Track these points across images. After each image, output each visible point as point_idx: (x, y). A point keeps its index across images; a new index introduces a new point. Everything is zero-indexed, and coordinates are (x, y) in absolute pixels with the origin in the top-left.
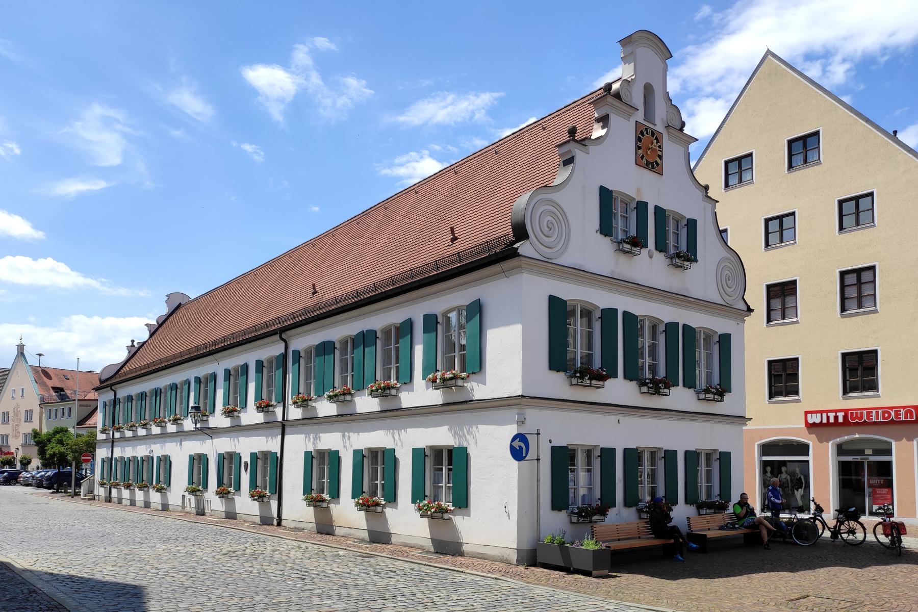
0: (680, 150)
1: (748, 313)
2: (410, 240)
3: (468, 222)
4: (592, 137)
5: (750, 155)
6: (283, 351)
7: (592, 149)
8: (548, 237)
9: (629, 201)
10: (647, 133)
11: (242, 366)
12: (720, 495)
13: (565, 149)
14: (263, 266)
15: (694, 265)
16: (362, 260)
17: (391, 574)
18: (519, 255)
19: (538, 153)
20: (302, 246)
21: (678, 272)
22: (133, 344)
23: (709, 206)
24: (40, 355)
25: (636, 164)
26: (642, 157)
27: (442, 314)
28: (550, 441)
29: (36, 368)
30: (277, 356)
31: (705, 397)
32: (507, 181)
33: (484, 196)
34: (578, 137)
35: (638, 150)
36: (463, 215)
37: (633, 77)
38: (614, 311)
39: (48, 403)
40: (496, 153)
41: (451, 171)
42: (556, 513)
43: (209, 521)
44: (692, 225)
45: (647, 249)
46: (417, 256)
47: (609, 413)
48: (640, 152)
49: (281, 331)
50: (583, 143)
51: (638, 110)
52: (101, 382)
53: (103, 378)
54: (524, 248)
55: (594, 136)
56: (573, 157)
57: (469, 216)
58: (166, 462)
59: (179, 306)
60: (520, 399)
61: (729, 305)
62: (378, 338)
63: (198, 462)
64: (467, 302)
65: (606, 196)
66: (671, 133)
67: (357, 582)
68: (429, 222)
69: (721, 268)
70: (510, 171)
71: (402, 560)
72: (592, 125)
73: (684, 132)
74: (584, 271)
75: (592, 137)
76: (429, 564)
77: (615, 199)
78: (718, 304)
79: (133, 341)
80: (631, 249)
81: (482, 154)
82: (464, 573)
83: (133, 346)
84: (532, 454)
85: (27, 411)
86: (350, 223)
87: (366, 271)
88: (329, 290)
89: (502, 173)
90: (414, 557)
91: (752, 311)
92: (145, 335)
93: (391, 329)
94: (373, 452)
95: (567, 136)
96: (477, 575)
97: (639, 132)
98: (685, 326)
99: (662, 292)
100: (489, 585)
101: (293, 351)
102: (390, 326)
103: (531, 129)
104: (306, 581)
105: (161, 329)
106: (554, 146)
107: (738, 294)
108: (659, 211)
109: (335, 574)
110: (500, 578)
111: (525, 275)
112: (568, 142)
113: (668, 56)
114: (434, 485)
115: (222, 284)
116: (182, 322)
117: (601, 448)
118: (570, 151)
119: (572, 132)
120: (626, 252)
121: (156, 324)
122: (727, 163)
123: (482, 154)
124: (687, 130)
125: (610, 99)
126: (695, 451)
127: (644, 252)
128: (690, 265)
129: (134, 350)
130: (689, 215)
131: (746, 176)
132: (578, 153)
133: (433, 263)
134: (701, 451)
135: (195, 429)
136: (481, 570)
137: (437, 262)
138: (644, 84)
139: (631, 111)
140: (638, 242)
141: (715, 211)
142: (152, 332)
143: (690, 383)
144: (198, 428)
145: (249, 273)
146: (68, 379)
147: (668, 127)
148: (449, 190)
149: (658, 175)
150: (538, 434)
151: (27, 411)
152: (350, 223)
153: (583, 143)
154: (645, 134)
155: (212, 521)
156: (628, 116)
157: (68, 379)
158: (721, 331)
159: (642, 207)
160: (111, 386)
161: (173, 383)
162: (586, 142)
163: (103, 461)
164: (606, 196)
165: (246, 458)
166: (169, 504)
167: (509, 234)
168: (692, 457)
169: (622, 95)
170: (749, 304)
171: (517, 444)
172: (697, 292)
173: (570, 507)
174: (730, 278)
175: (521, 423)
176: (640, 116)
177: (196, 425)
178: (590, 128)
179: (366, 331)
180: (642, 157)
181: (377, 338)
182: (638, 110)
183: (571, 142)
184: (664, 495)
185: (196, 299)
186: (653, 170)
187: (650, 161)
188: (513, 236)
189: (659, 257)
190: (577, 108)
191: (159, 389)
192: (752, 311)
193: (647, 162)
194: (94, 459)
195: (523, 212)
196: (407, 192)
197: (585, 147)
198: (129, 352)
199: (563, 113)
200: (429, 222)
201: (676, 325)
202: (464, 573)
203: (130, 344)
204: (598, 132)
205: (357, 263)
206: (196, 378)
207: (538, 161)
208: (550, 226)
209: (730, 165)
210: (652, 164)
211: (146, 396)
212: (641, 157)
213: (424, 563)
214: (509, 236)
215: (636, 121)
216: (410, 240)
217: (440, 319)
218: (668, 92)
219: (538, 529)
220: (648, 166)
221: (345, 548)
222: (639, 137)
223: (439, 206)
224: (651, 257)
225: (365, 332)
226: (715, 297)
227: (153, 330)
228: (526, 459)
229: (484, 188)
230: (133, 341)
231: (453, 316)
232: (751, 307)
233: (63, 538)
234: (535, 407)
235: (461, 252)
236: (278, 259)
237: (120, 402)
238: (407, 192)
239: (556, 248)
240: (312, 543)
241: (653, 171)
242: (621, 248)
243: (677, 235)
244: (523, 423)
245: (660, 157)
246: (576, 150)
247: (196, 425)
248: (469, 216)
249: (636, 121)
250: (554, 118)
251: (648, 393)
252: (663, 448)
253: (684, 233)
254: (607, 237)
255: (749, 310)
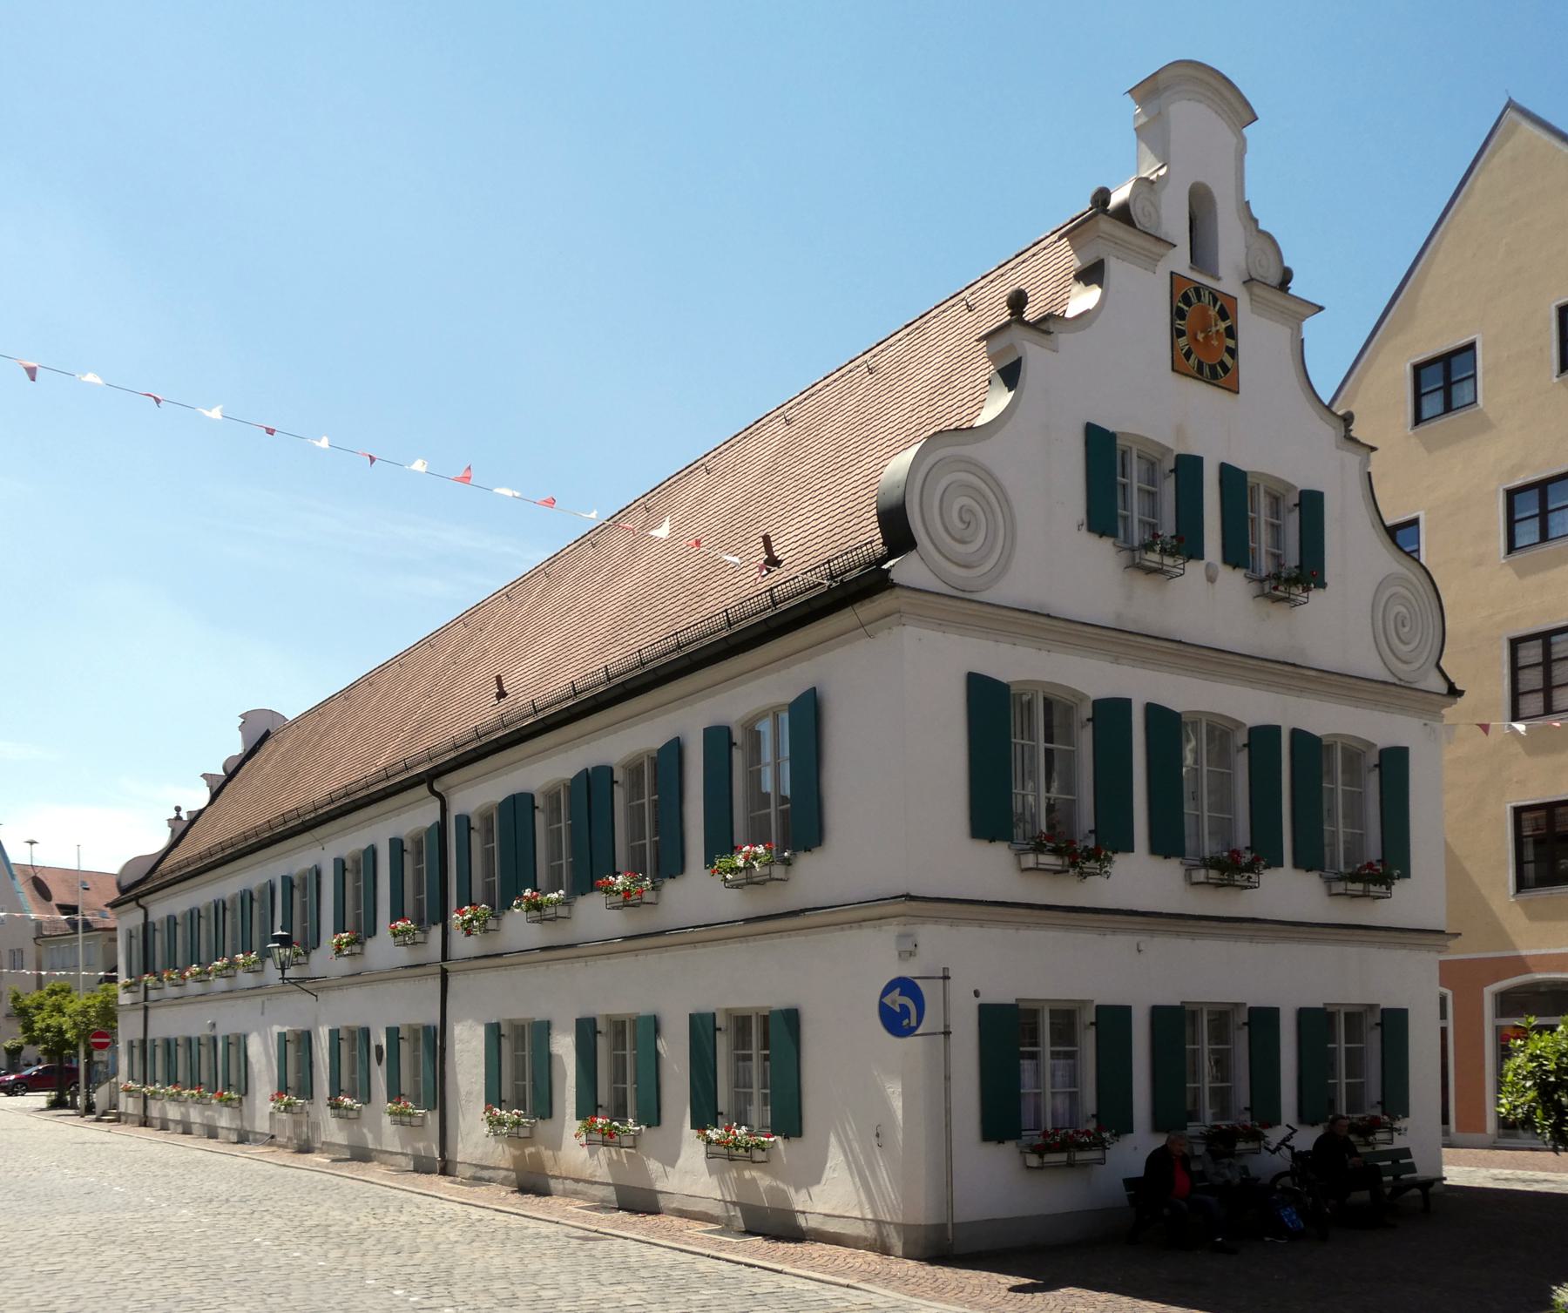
0: (1282, 333)
1: (1450, 700)
2: (688, 572)
3: (803, 523)
4: (1068, 315)
5: (1471, 347)
6: (438, 817)
7: (1063, 338)
8: (962, 542)
9: (1159, 457)
10: (1199, 299)
11: (365, 852)
12: (1382, 1103)
13: (1002, 342)
14: (417, 646)
15: (1316, 595)
16: (595, 621)
17: (624, 1276)
18: (893, 586)
19: (955, 361)
20: (488, 601)
21: (1278, 611)
22: (178, 814)
23: (1352, 459)
24: (32, 843)
25: (1173, 370)
26: (1188, 355)
27: (742, 726)
28: (977, 994)
29: (26, 868)
30: (429, 829)
31: (1208, 878)
32: (887, 428)
33: (839, 464)
34: (1030, 314)
35: (1179, 337)
36: (795, 510)
37: (1162, 172)
38: (1123, 705)
39: (50, 936)
40: (871, 371)
41: (778, 419)
42: (992, 1149)
43: (313, 1164)
44: (1311, 504)
45: (1202, 564)
46: (699, 604)
47: (1114, 931)
48: (1182, 341)
49: (430, 778)
50: (1044, 327)
51: (1175, 246)
52: (123, 891)
53: (125, 883)
54: (902, 568)
55: (1072, 311)
56: (1020, 360)
57: (806, 510)
58: (238, 1043)
59: (267, 735)
60: (903, 902)
61: (1402, 683)
62: (617, 782)
63: (298, 1045)
64: (790, 697)
65: (1100, 445)
66: (1258, 296)
67: (540, 1293)
68: (728, 531)
69: (1382, 604)
70: (895, 406)
71: (664, 1247)
72: (1068, 289)
73: (1290, 292)
74: (1048, 616)
75: (1067, 315)
76: (716, 1254)
77: (1124, 453)
78: (1376, 681)
79: (178, 809)
80: (1289, 593)
81: (843, 376)
82: (786, 1273)
83: (178, 818)
84: (931, 1021)
85: (12, 952)
86: (580, 546)
87: (599, 642)
88: (528, 687)
89: (879, 411)
90: (691, 1241)
91: (1460, 693)
92: (198, 797)
93: (642, 764)
94: (616, 1023)
95: (1006, 314)
96: (811, 1279)
97: (1178, 296)
98: (1295, 733)
99: (1237, 658)
100: (825, 1300)
101: (456, 816)
102: (640, 756)
103: (944, 312)
104: (435, 1289)
105: (230, 785)
106: (977, 337)
107: (1425, 657)
108: (1232, 478)
109: (505, 1276)
110: (856, 1285)
111: (909, 629)
112: (1006, 326)
113: (1248, 118)
114: (736, 1089)
115: (343, 688)
116: (268, 768)
117: (1097, 1006)
118: (1012, 347)
119: (1018, 301)
120: (1150, 571)
121: (223, 774)
122: (1418, 369)
123: (843, 376)
124: (1295, 288)
125: (1105, 225)
126: (1324, 1009)
127: (1194, 569)
128: (1182, 566)
129: (181, 828)
130: (1304, 481)
131: (1461, 393)
132: (1033, 353)
133: (721, 615)
134: (1337, 1008)
135: (281, 981)
136: (821, 1269)
137: (729, 611)
138: (1188, 187)
139: (1157, 248)
140: (1188, 545)
141: (1369, 470)
142: (214, 791)
143: (1308, 859)
144: (287, 979)
145: (390, 663)
146: (87, 889)
147: (1249, 281)
148: (772, 459)
149: (1227, 392)
150: (946, 978)
151: (12, 952)
152: (580, 546)
153: (1044, 327)
154: (1194, 299)
155: (318, 1164)
156: (1152, 261)
157: (87, 889)
158: (1383, 740)
159: (1188, 468)
160: (137, 898)
161: (244, 890)
162: (1051, 326)
163: (131, 1045)
164: (1100, 445)
165: (380, 1038)
166: (216, 1127)
167: (873, 541)
168: (1315, 1022)
169: (1136, 213)
170: (1453, 681)
171: (897, 1000)
172: (1325, 655)
173: (1023, 1133)
174: (1408, 622)
175: (908, 954)
176: (1180, 260)
177: (283, 973)
178: (1066, 296)
179: (593, 768)
180: (1188, 355)
181: (613, 782)
182: (1175, 246)
183: (1013, 325)
184: (1248, 1106)
185: (296, 721)
186: (1215, 382)
187: (1207, 361)
188: (883, 544)
189: (1234, 582)
190: (1040, 255)
191: (221, 903)
192: (1460, 693)
193: (1200, 364)
194: (115, 1042)
195: (902, 488)
196: (691, 472)
197: (1048, 337)
198: (173, 831)
199: (1012, 269)
200: (728, 531)
201: (1275, 731)
202: (786, 1273)
203: (173, 815)
204: (1084, 299)
205: (584, 627)
206: (284, 878)
207: (953, 379)
208: (967, 517)
209: (1424, 372)
210: (1213, 368)
211: (199, 917)
212: (1185, 355)
213: (707, 1252)
214: (873, 544)
215: (1172, 273)
216: (688, 572)
217: (738, 736)
218: (1248, 203)
219: (950, 1184)
220: (1202, 374)
221: (556, 1220)
222: (1178, 308)
223: (749, 495)
224: (1211, 579)
225: (590, 769)
226: (1375, 669)
227: (215, 788)
228: (917, 1032)
229: (840, 449)
230: (178, 809)
231: (765, 727)
232: (1459, 687)
233: (10, 1196)
234: (937, 919)
235: (776, 587)
236: (446, 628)
237: (155, 930)
238: (691, 472)
239: (978, 569)
240: (496, 1210)
241: (1214, 385)
242: (1137, 560)
243: (1276, 529)
244: (911, 954)
245: (1233, 353)
246: (1025, 342)
247: (283, 973)
248: (806, 510)
249: (1172, 273)
250: (992, 282)
251: (1208, 883)
252: (1245, 1004)
253: (1292, 523)
254: (1104, 538)
255: (1454, 692)
